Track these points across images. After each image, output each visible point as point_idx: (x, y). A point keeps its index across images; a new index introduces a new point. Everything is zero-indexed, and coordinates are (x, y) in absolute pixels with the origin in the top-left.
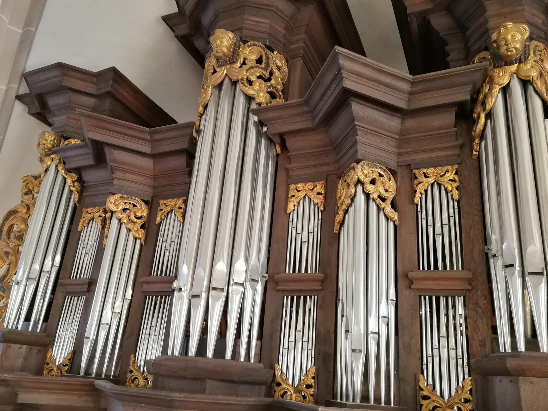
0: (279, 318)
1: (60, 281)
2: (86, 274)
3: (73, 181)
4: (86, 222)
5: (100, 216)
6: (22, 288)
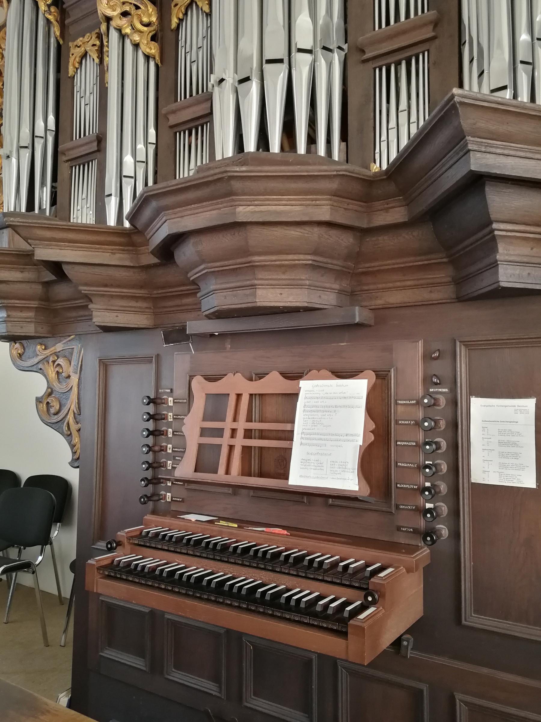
0: (370, 101)
1: (61, 147)
2: (92, 130)
3: (47, 5)
4: (78, 59)
5: (94, 45)
6: (14, 160)
